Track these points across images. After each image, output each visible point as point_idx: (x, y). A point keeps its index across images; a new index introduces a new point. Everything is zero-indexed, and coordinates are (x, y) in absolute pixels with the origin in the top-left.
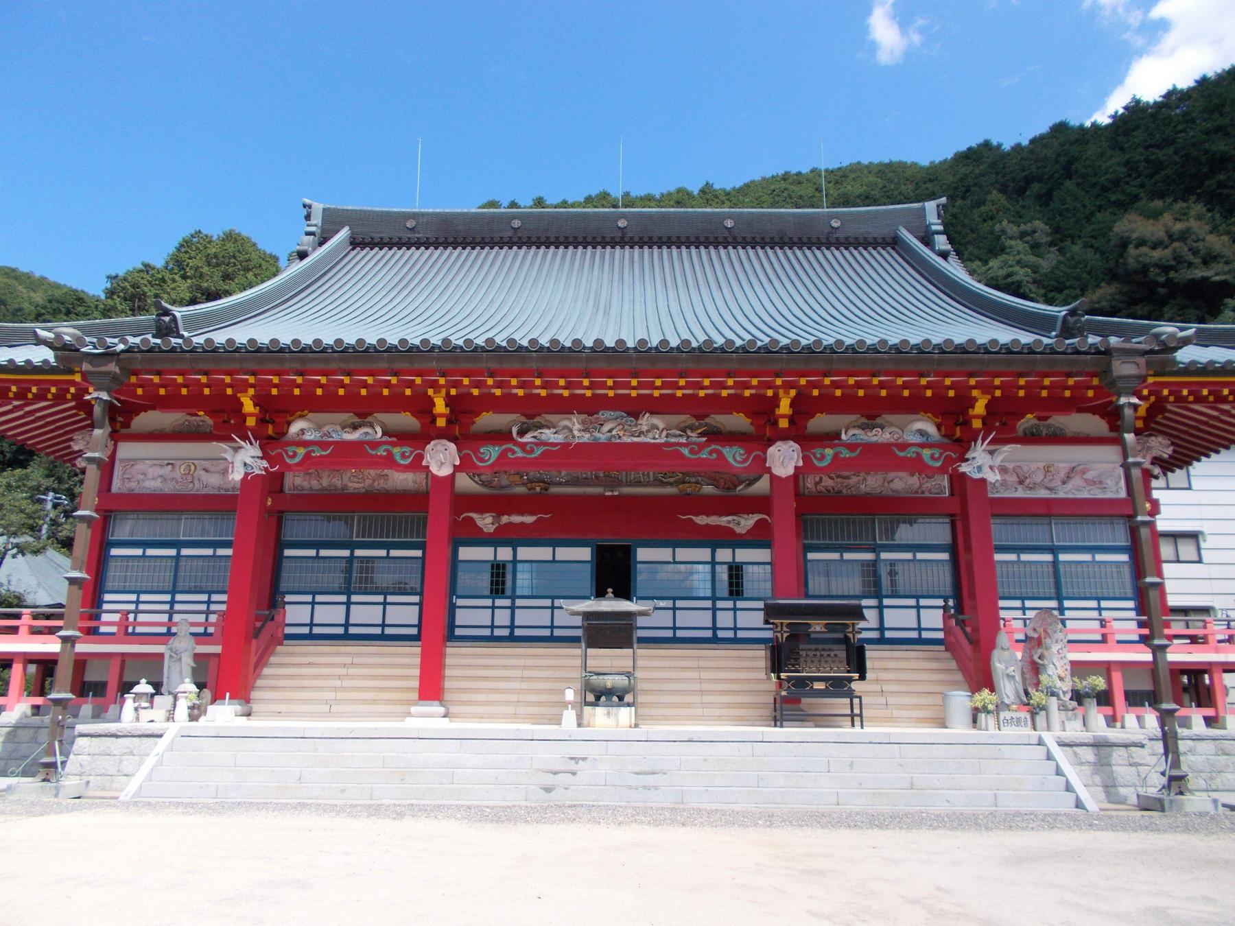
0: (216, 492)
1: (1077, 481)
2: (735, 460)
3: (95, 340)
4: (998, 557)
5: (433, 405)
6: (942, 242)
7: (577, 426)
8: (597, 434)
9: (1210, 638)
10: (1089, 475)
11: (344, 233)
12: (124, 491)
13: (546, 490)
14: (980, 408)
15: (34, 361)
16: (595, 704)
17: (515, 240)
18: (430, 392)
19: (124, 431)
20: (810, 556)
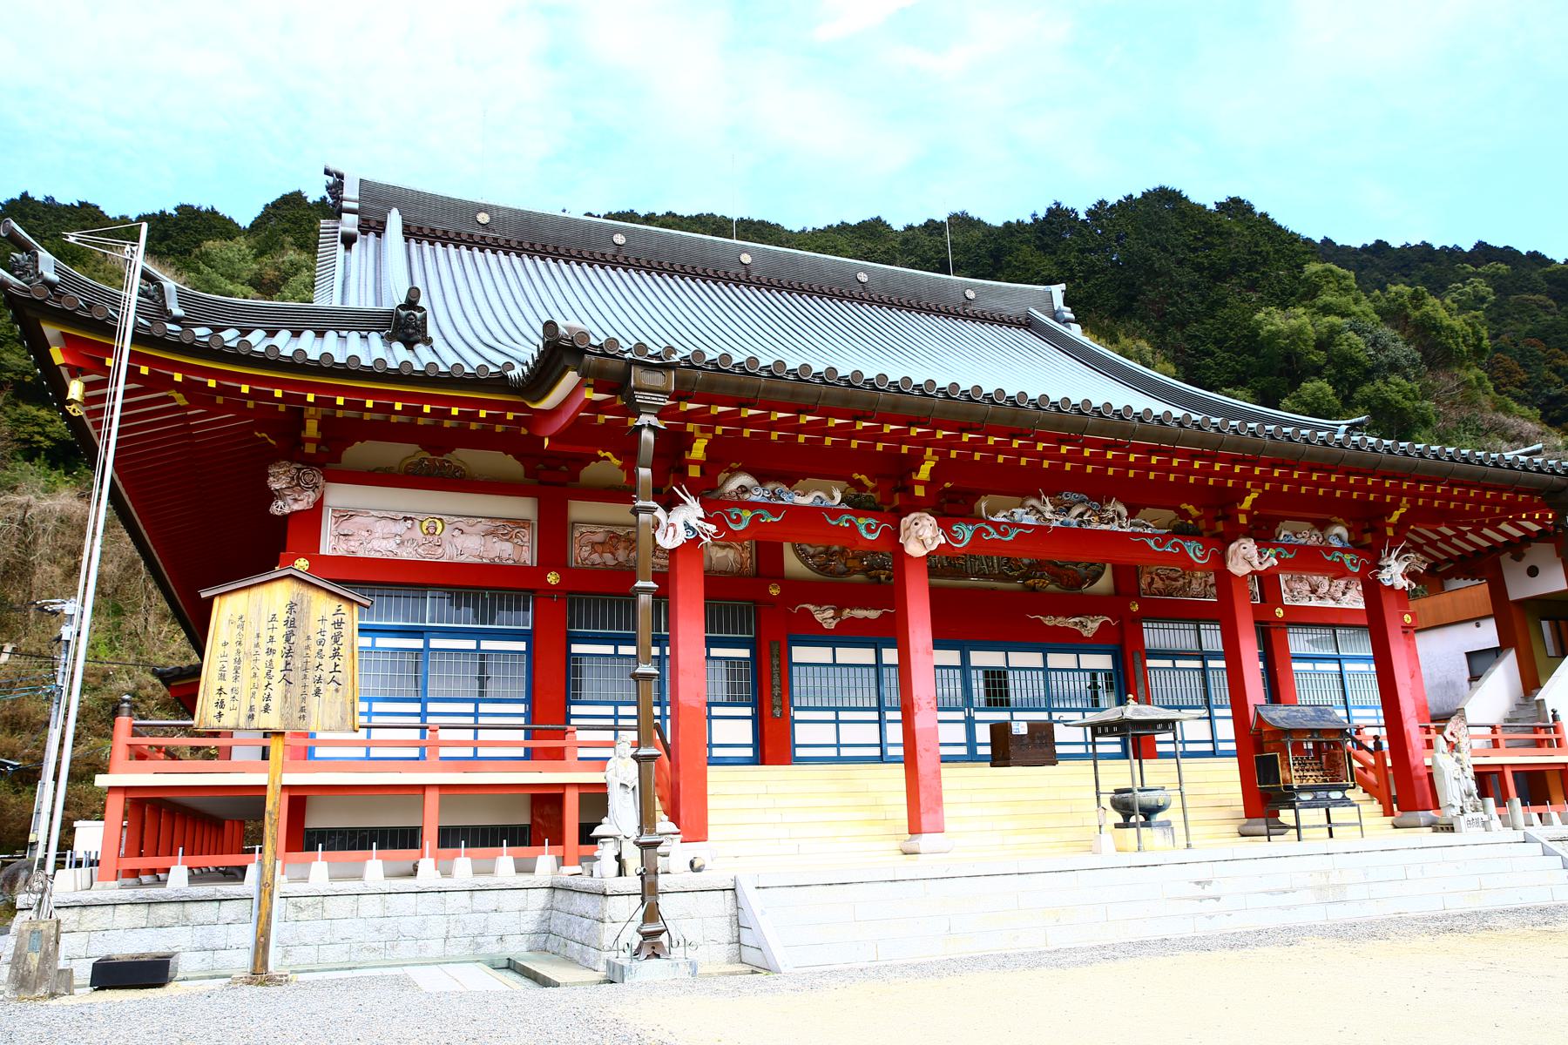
0: (478, 560)
4: (1150, 663)
7: (1050, 507)
9: (568, 753)
20: (576, 649)
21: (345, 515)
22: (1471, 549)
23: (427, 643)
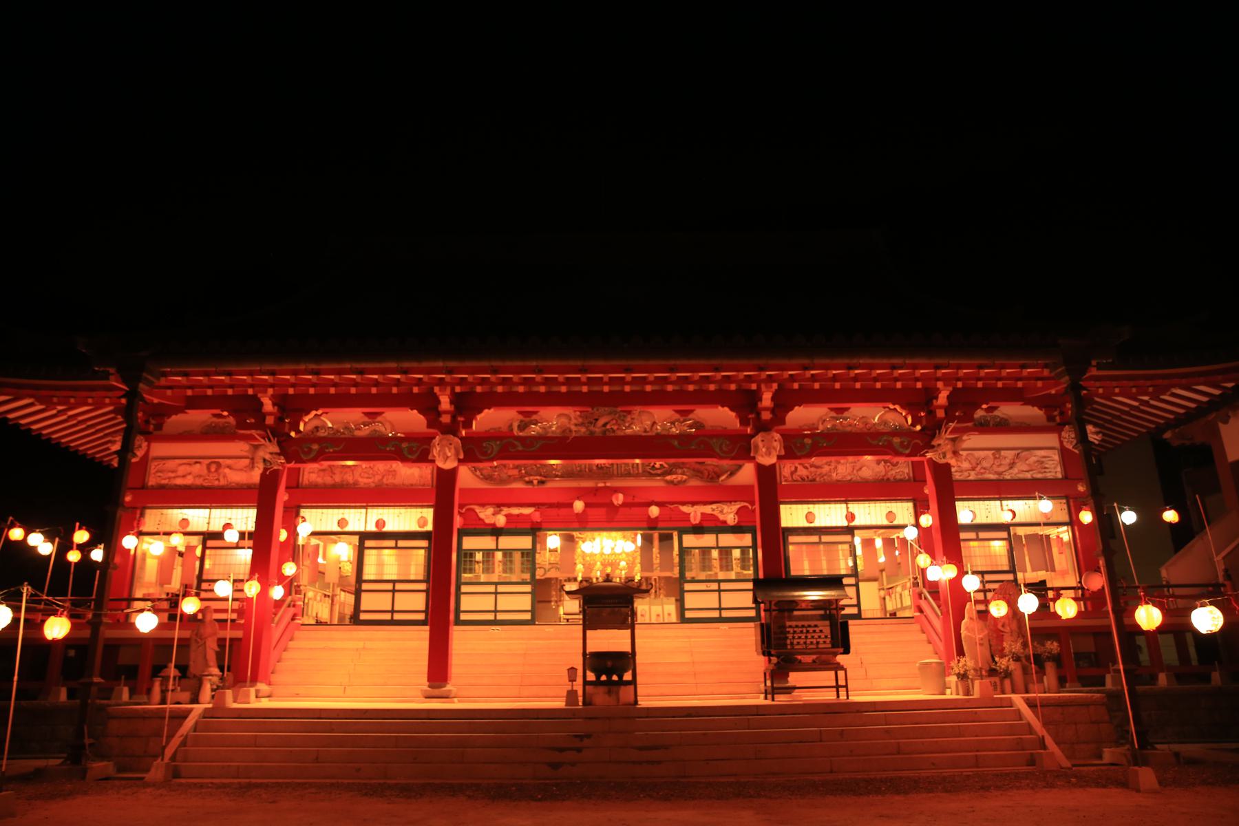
2: (721, 449)
5: (439, 402)
8: (592, 428)
14: (942, 398)
18: (436, 389)
19: (158, 433)
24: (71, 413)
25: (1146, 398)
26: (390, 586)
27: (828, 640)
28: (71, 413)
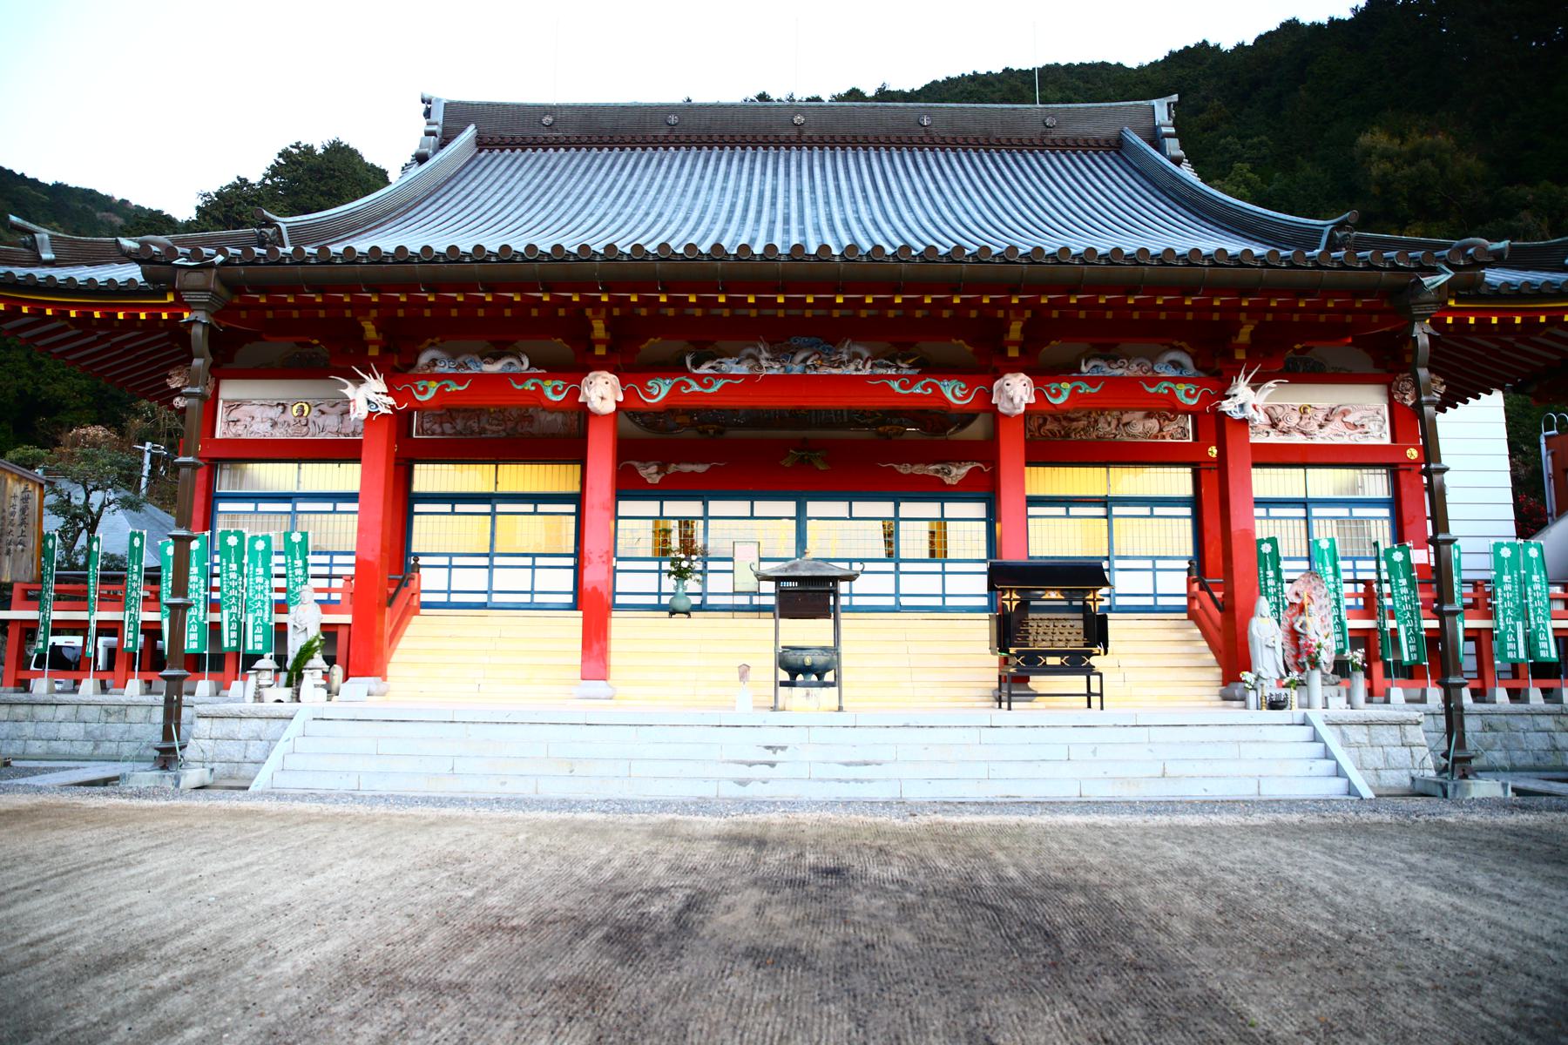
1: (1336, 424)
3: (188, 251)
5: (592, 328)
6: (1173, 146)
10: (1349, 419)
11: (471, 131)
12: (230, 436)
13: (721, 432)
14: (1244, 335)
15: (78, 279)
16: (791, 684)
17: (672, 139)
18: (589, 312)
21: (234, 405)
22: (1541, 364)
23: (294, 507)
24: (115, 340)
25: (1510, 339)
26: (445, 561)
27: (1081, 637)
28: (115, 340)
